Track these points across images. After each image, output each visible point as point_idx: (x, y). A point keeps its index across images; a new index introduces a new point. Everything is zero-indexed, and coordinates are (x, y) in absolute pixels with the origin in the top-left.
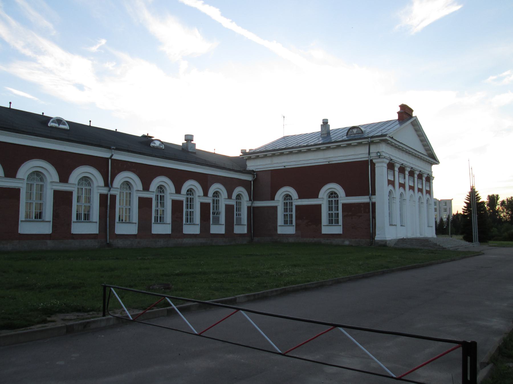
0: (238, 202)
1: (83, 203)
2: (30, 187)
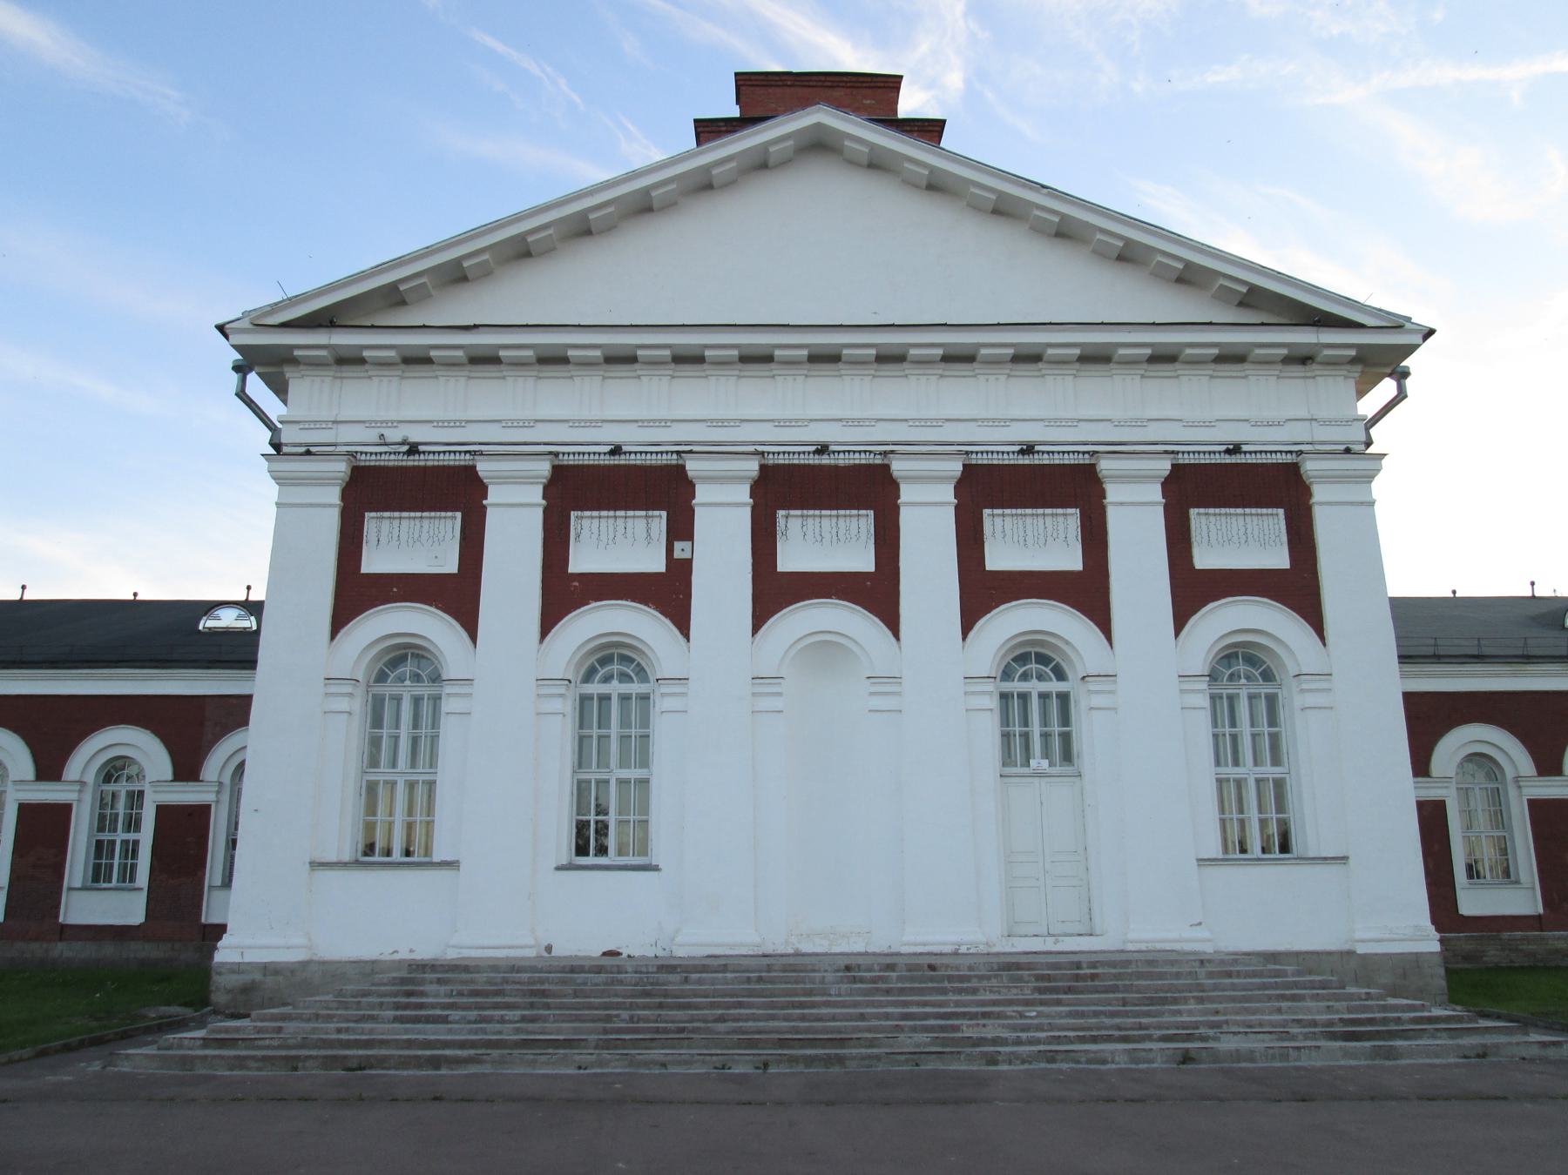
1: (1482, 830)
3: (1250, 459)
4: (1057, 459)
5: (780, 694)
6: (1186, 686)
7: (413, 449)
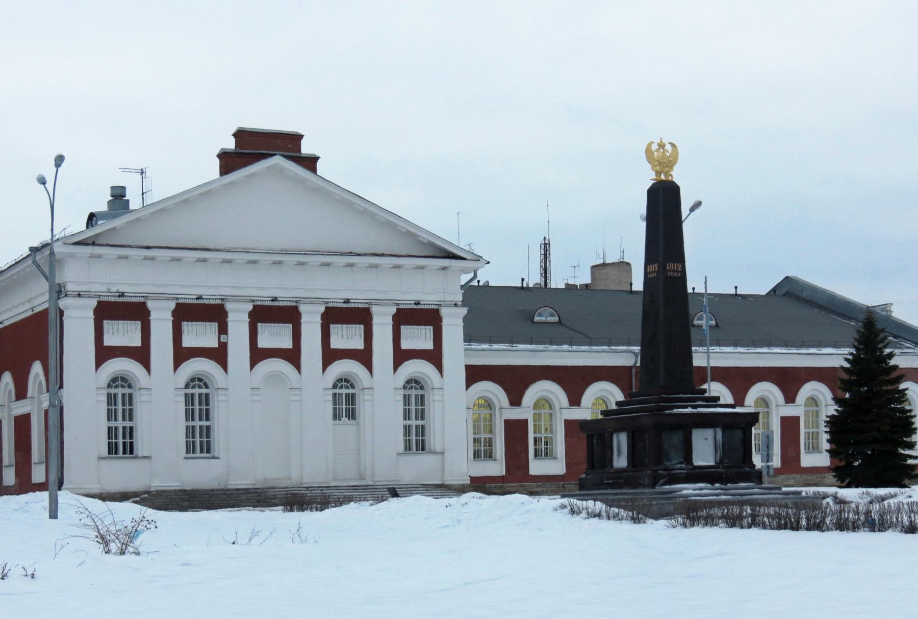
0: (811, 433)
2: (537, 417)
3: (423, 307)
4: (357, 305)
5: (259, 394)
6: (99, 392)
7: (122, 295)
